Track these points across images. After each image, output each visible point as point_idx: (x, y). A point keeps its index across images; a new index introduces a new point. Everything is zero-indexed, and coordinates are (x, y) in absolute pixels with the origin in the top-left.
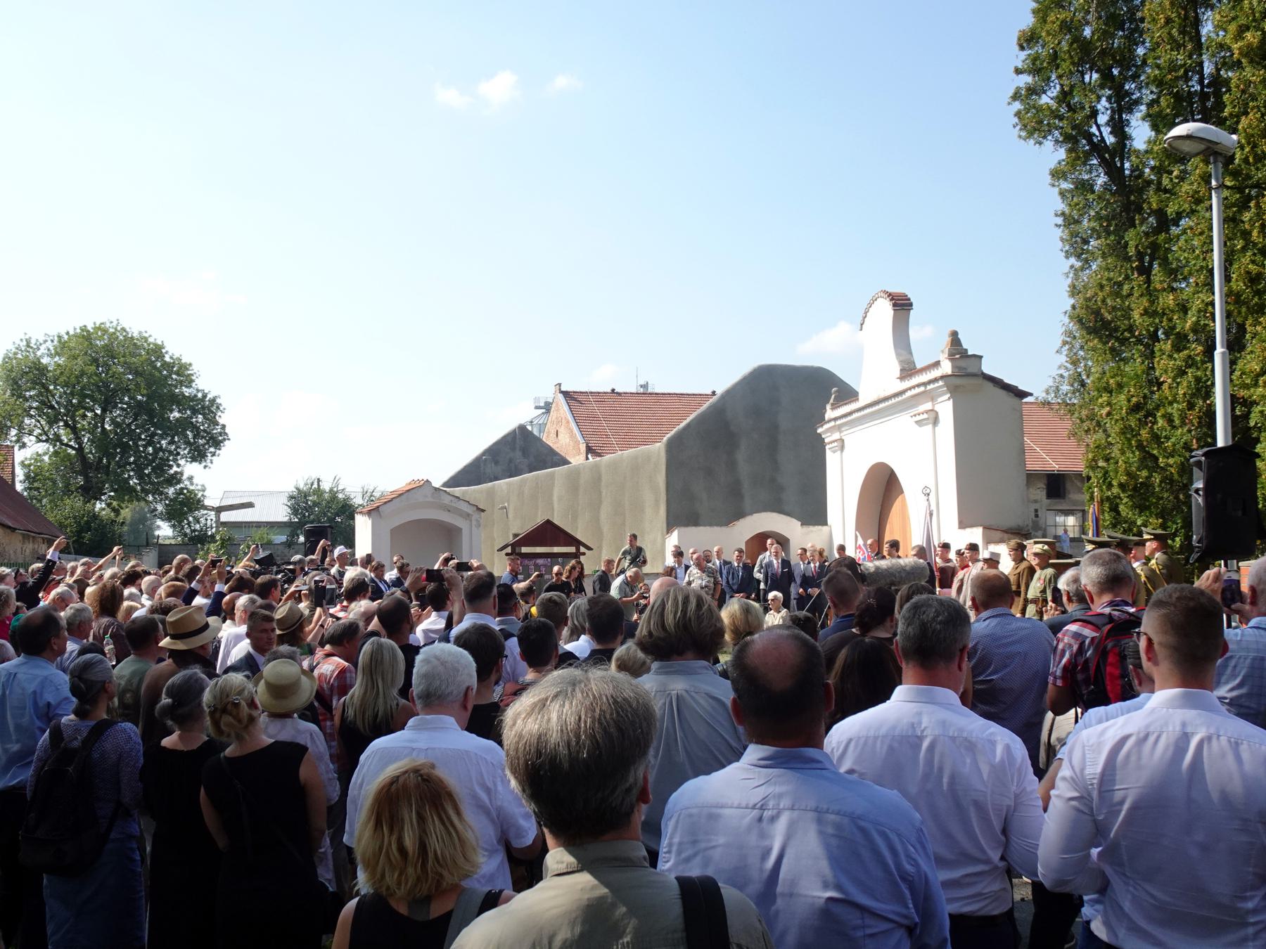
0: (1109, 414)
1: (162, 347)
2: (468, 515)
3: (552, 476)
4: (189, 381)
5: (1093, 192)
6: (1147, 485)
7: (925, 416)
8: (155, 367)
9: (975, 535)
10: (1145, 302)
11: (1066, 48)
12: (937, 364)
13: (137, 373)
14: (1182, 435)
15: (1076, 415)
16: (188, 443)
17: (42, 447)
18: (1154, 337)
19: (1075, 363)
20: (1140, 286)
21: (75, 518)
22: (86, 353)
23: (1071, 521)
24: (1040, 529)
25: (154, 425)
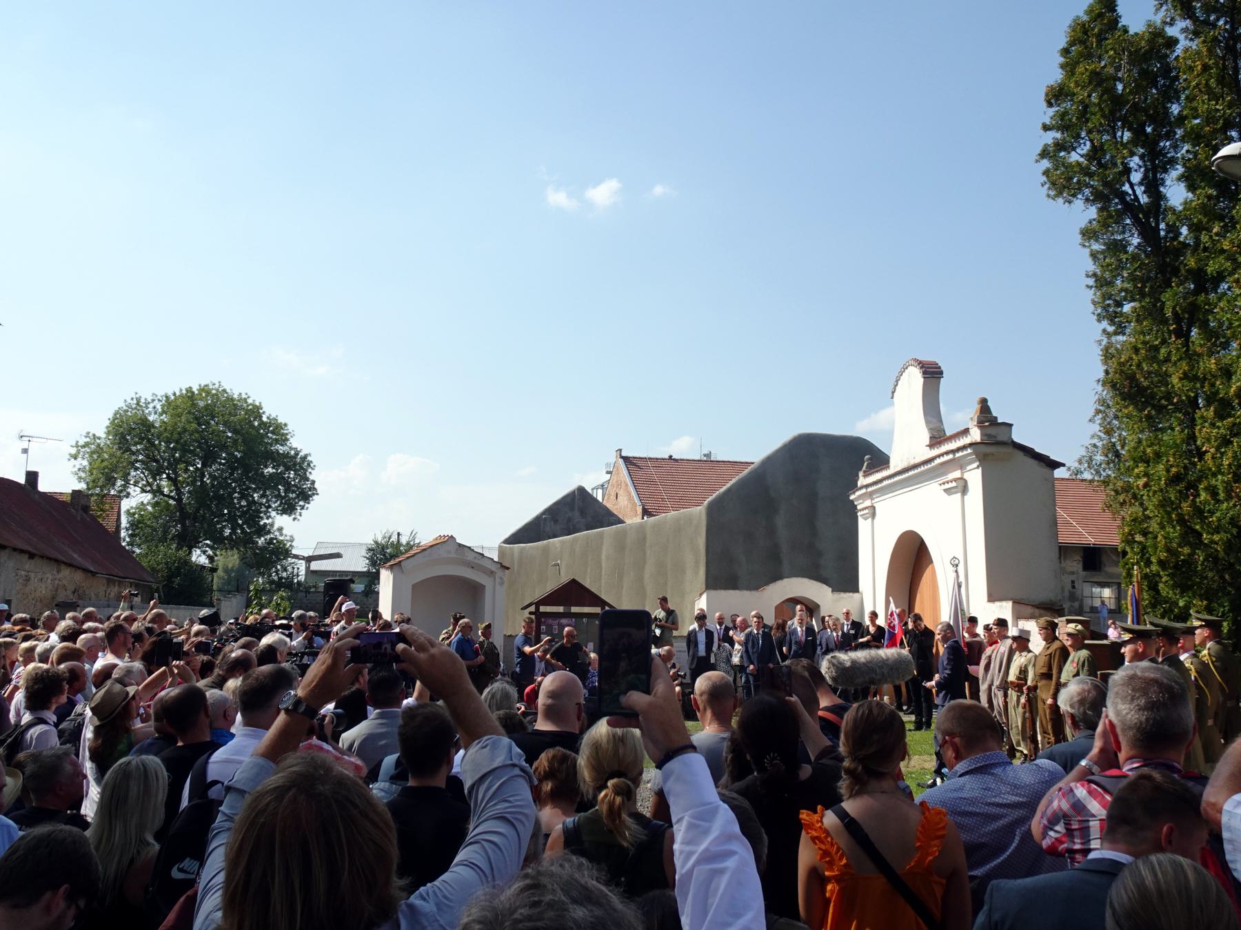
0: (1146, 485)
1: (259, 408)
2: (492, 572)
3: (601, 536)
4: (283, 440)
5: (1126, 252)
6: (1189, 562)
7: (954, 484)
8: (253, 426)
9: (1004, 610)
10: (1184, 366)
11: (1096, 101)
12: (966, 432)
13: (235, 431)
14: (1228, 509)
15: (1111, 486)
16: (278, 496)
17: (147, 498)
18: (1193, 403)
19: (1109, 432)
20: (1178, 349)
21: (167, 563)
22: (189, 413)
23: (1107, 593)
24: (1077, 599)
25: (248, 478)
